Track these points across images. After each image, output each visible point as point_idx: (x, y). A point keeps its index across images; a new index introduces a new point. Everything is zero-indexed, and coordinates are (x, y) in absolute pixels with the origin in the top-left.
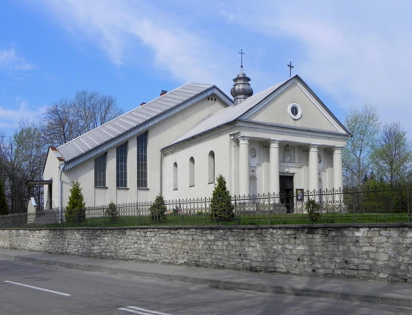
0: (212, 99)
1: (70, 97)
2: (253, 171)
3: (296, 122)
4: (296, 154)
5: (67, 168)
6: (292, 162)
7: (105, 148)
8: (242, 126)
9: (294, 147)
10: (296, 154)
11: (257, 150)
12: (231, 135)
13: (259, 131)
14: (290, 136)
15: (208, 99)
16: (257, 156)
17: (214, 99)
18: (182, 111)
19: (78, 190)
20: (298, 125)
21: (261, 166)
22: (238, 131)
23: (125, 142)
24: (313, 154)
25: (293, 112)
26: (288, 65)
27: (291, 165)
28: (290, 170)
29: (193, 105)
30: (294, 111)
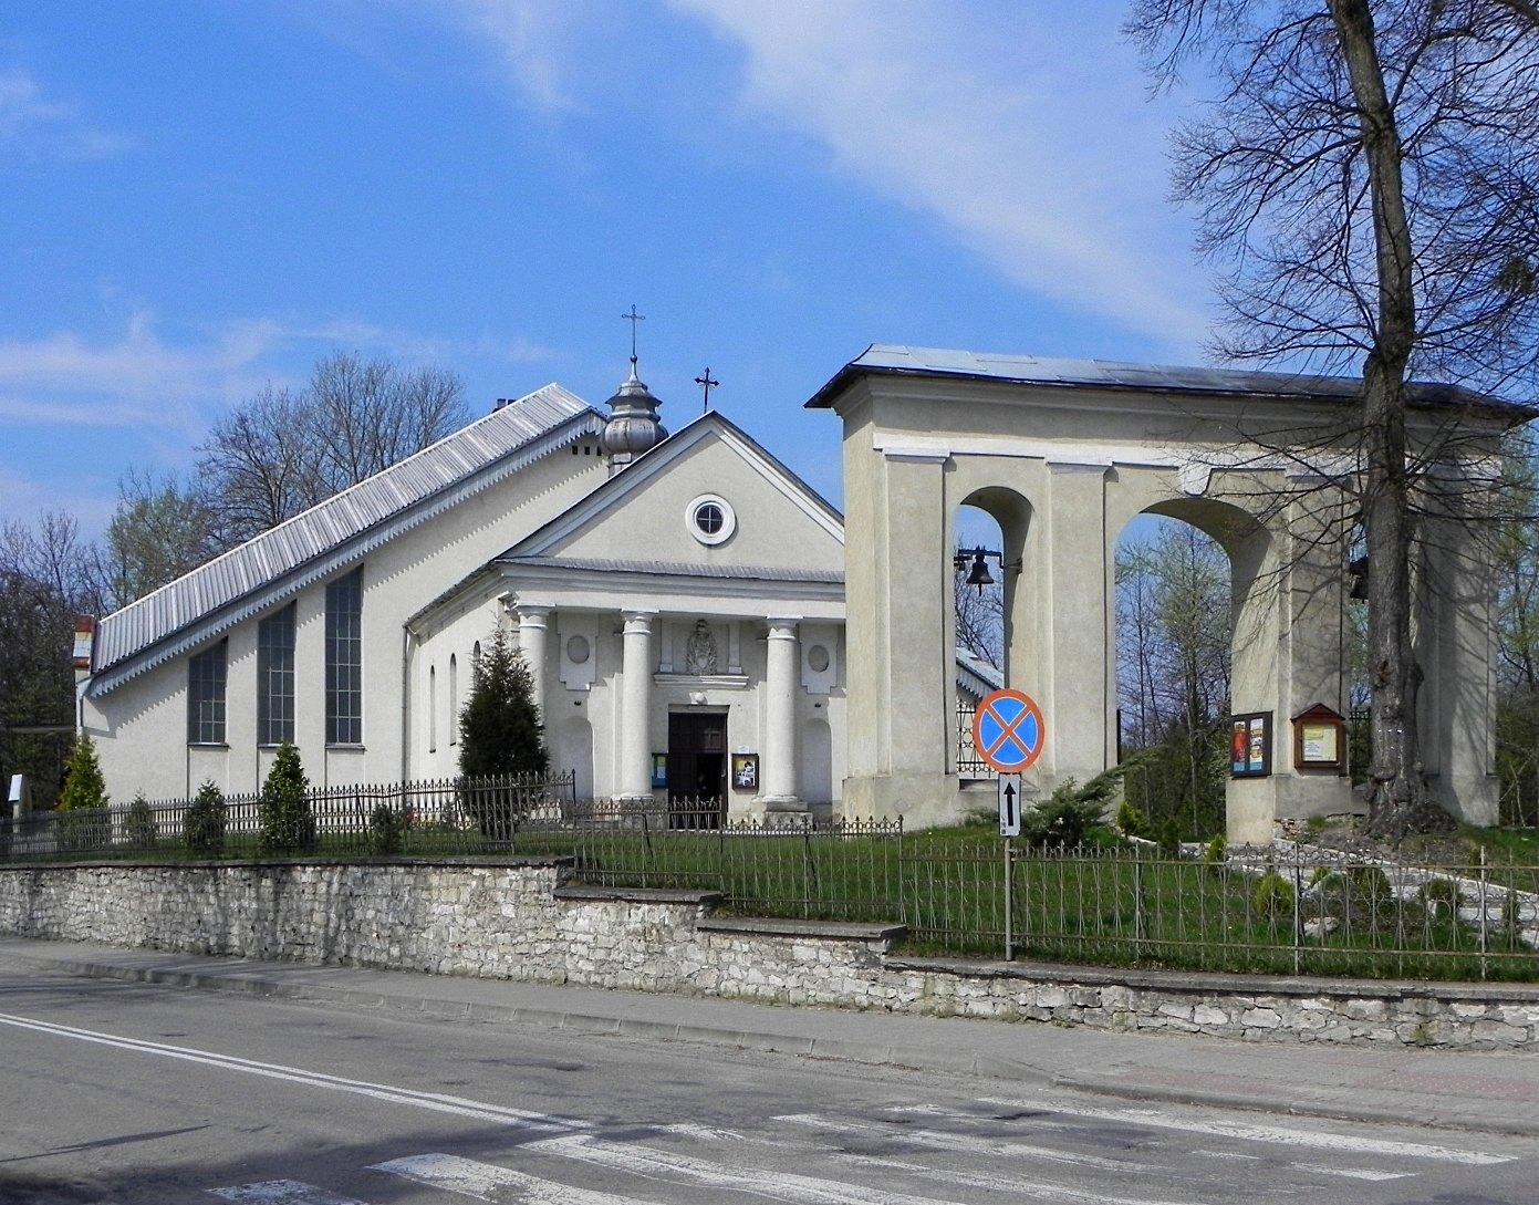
0: (587, 452)
1: (293, 385)
2: (578, 704)
3: (713, 551)
4: (734, 648)
5: (99, 689)
6: (719, 670)
7: (216, 627)
8: (520, 577)
9: (728, 626)
10: (734, 648)
11: (591, 641)
12: (502, 600)
13: (576, 589)
14: (690, 598)
15: (575, 451)
16: (592, 659)
17: (594, 450)
18: (480, 497)
19: (89, 761)
20: (723, 560)
21: (605, 684)
22: (507, 592)
23: (285, 604)
24: (779, 648)
25: (704, 526)
26: (698, 380)
27: (708, 680)
28: (707, 694)
29: (519, 475)
30: (709, 519)
